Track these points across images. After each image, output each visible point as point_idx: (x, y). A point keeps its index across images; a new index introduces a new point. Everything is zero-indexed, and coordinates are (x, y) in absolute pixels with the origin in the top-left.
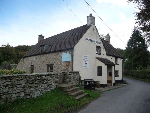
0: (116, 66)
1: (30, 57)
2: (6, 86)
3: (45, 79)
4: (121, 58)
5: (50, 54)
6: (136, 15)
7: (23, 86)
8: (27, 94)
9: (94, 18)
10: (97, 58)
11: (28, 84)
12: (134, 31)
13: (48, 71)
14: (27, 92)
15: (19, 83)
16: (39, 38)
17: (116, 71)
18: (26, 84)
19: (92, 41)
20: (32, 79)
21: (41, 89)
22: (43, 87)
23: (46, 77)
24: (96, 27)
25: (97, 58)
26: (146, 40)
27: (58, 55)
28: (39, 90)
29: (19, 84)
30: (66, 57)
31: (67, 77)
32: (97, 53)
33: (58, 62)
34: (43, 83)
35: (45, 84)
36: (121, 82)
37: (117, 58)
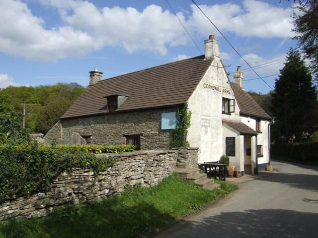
0: (259, 135)
1: (79, 120)
4: (265, 119)
5: (131, 114)
6: (295, 19)
10: (224, 122)
12: (289, 56)
15: (140, 165)
19: (215, 88)
25: (224, 122)
26: (312, 75)
32: (223, 112)
33: (152, 131)
37: (258, 119)
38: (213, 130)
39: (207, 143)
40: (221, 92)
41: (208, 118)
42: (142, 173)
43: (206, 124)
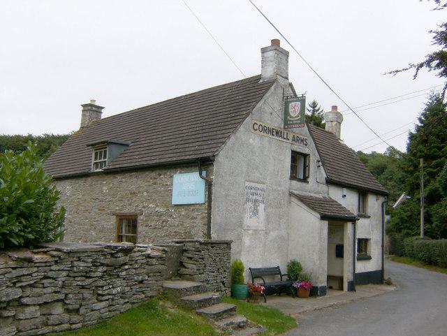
0: (361, 223)
2: (17, 282)
3: (125, 264)
4: (377, 193)
7: (60, 283)
8: (70, 307)
9: (286, 54)
11: (74, 277)
13: (120, 238)
14: (72, 302)
15: (50, 274)
16: (84, 115)
17: (360, 240)
18: (68, 276)
19: (277, 133)
20: (87, 262)
21: (111, 297)
22: (119, 289)
23: (128, 258)
24: (291, 85)
27: (158, 181)
28: (107, 297)
29: (50, 278)
30: (187, 186)
31: (191, 258)
33: (157, 206)
34: (118, 276)
35: (124, 279)
36: (377, 278)
37: (363, 193)
38: (269, 210)
39: (256, 231)
40: (290, 141)
41: (260, 186)
42: (56, 292)
43: (254, 197)
